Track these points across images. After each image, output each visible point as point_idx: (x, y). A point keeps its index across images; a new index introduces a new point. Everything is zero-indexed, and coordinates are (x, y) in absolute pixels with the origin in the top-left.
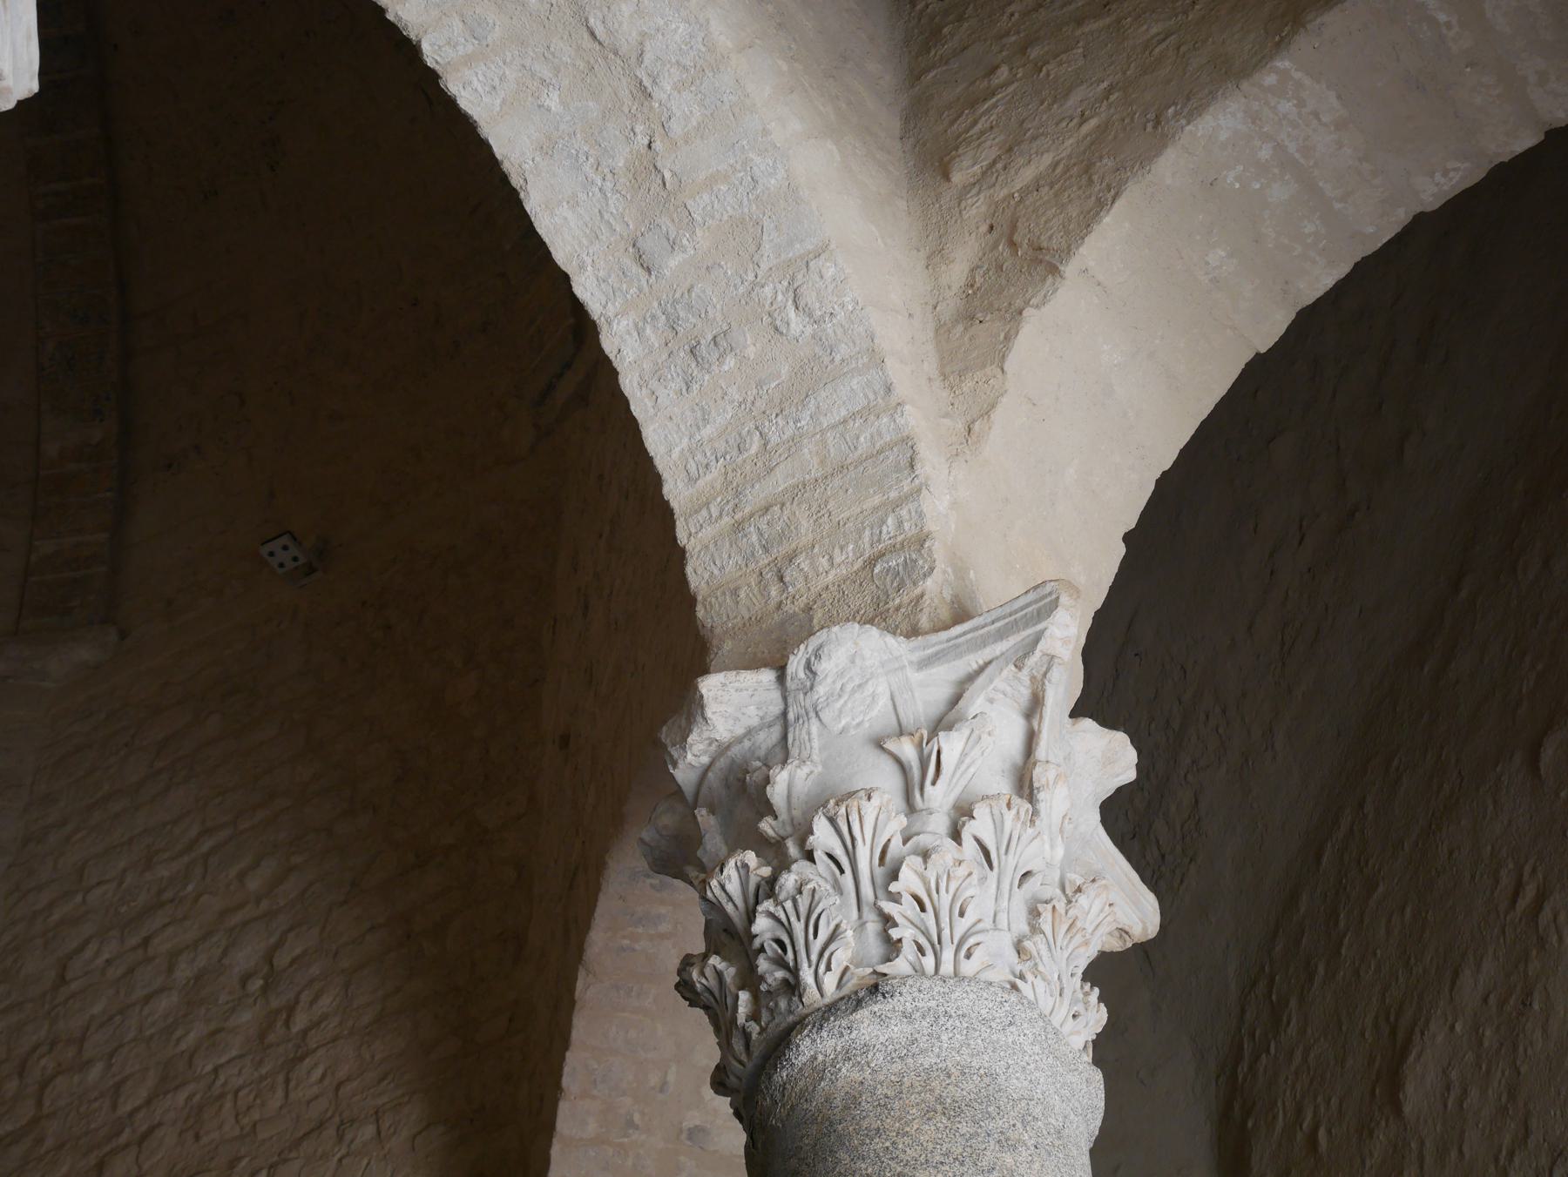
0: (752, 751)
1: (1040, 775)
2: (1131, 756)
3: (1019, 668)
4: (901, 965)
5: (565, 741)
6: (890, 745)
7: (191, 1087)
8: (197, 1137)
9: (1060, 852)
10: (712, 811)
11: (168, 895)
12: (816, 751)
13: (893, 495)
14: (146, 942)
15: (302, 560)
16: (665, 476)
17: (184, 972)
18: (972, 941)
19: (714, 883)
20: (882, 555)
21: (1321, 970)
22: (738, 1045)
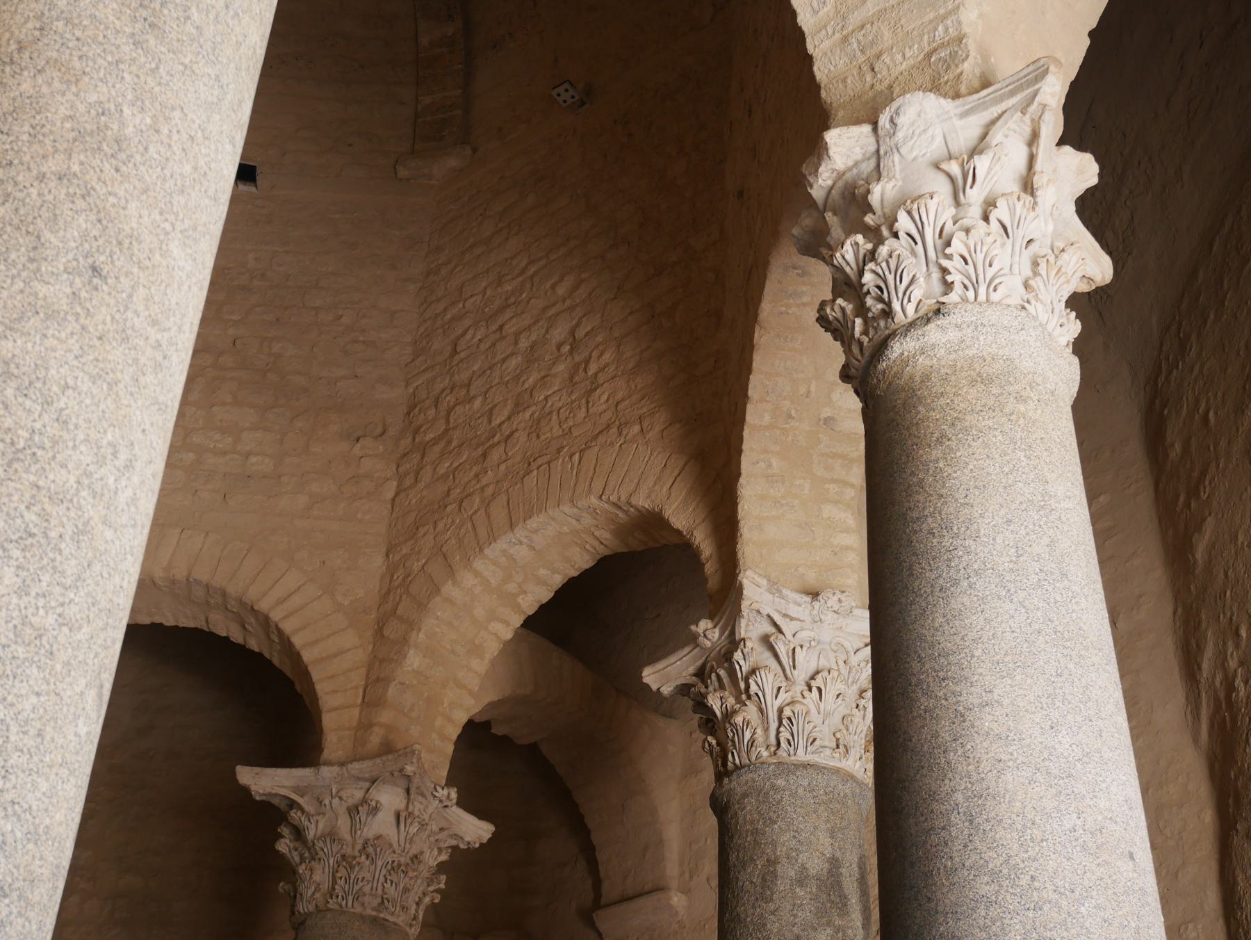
0: (858, 175)
1: (1037, 180)
2: (1095, 168)
3: (1024, 113)
4: (953, 297)
5: (740, 194)
6: (944, 166)
7: (533, 408)
8: (538, 437)
9: (1051, 228)
10: (835, 214)
11: (512, 300)
12: (898, 173)
13: (942, 11)
14: (501, 327)
15: (577, 98)
16: (799, 11)
17: (524, 344)
18: (997, 281)
19: (838, 255)
20: (935, 50)
21: (1212, 316)
22: (855, 350)
